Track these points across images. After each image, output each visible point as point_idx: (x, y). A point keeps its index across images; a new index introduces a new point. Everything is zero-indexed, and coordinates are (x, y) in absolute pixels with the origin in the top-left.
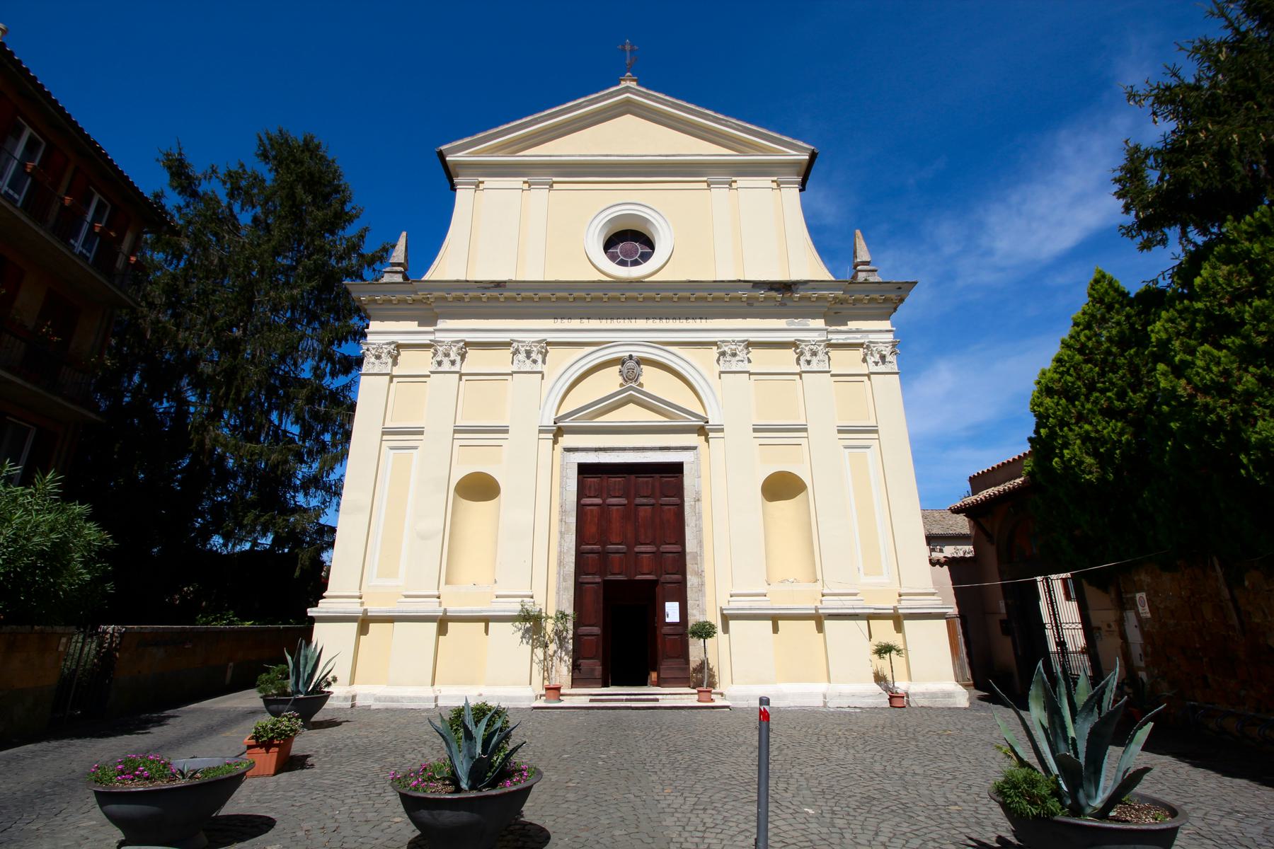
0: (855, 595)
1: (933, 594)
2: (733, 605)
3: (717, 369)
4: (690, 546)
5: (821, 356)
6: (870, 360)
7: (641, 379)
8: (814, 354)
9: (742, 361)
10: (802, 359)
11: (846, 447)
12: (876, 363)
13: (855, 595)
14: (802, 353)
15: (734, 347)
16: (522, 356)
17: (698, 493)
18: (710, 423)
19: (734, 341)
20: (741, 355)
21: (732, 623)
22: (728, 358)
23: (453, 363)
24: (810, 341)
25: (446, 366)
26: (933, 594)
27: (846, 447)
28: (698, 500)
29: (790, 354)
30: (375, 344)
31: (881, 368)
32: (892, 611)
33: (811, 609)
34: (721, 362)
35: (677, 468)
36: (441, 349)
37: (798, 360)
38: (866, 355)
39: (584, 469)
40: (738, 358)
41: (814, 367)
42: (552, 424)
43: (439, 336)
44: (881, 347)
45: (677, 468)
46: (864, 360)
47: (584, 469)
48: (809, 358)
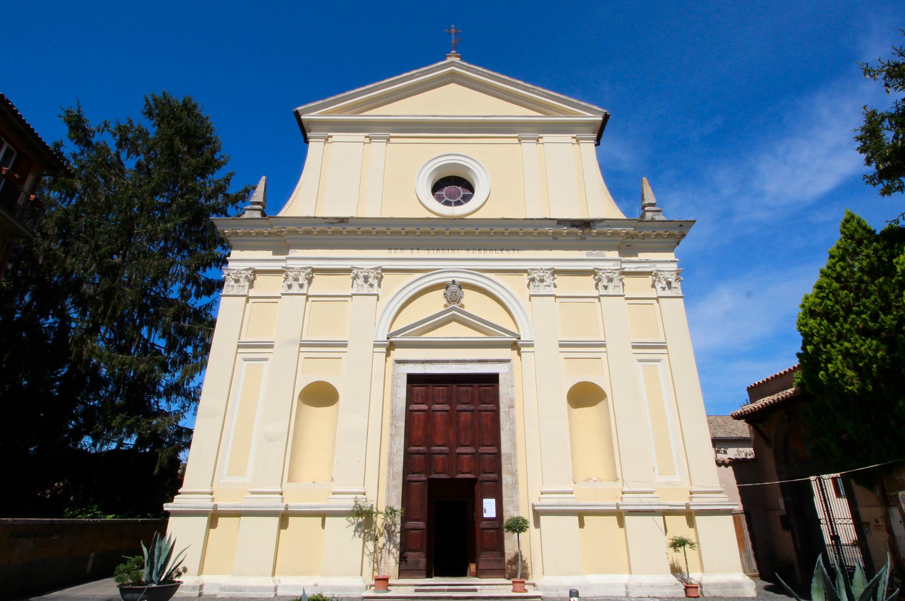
0: (651, 492)
1: (720, 492)
2: (544, 502)
3: (528, 292)
4: (505, 448)
5: (616, 282)
6: (659, 286)
7: (463, 301)
8: (610, 280)
9: (549, 286)
10: (600, 284)
11: (640, 361)
12: (664, 289)
13: (651, 492)
14: (600, 280)
15: (541, 274)
16: (360, 281)
17: (512, 400)
18: (522, 339)
19: (541, 269)
20: (548, 281)
21: (543, 519)
22: (537, 283)
23: (301, 286)
24: (606, 270)
25: (295, 289)
26: (720, 492)
27: (640, 361)
28: (512, 407)
29: (590, 280)
30: (234, 270)
31: (667, 293)
32: (685, 508)
33: (613, 506)
34: (531, 287)
35: (493, 379)
36: (291, 274)
37: (597, 285)
38: (654, 281)
39: (413, 380)
40: (545, 283)
41: (610, 291)
42: (385, 339)
43: (290, 264)
44: (667, 275)
45: (493, 379)
46: (653, 286)
47: (413, 380)
48: (606, 284)
